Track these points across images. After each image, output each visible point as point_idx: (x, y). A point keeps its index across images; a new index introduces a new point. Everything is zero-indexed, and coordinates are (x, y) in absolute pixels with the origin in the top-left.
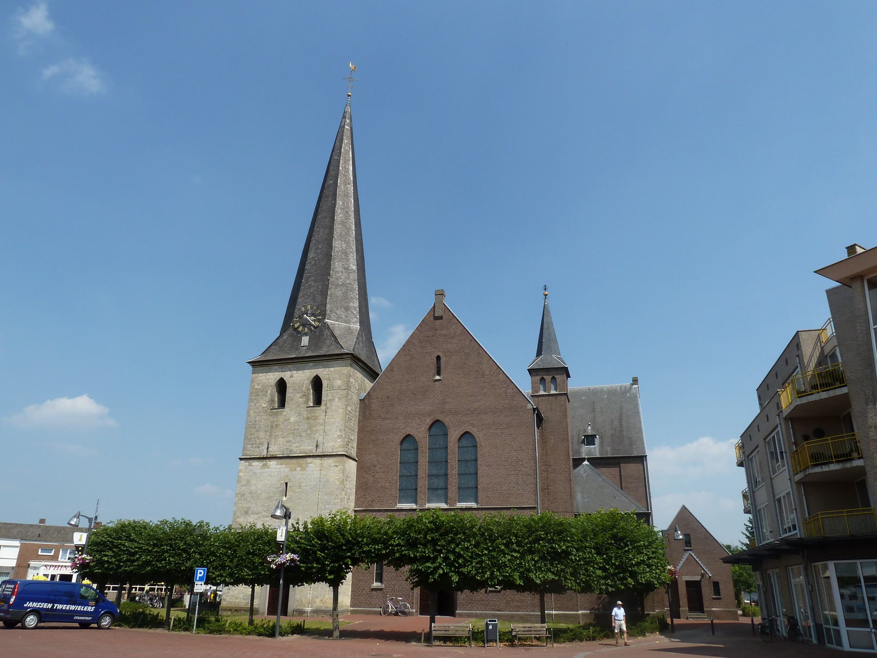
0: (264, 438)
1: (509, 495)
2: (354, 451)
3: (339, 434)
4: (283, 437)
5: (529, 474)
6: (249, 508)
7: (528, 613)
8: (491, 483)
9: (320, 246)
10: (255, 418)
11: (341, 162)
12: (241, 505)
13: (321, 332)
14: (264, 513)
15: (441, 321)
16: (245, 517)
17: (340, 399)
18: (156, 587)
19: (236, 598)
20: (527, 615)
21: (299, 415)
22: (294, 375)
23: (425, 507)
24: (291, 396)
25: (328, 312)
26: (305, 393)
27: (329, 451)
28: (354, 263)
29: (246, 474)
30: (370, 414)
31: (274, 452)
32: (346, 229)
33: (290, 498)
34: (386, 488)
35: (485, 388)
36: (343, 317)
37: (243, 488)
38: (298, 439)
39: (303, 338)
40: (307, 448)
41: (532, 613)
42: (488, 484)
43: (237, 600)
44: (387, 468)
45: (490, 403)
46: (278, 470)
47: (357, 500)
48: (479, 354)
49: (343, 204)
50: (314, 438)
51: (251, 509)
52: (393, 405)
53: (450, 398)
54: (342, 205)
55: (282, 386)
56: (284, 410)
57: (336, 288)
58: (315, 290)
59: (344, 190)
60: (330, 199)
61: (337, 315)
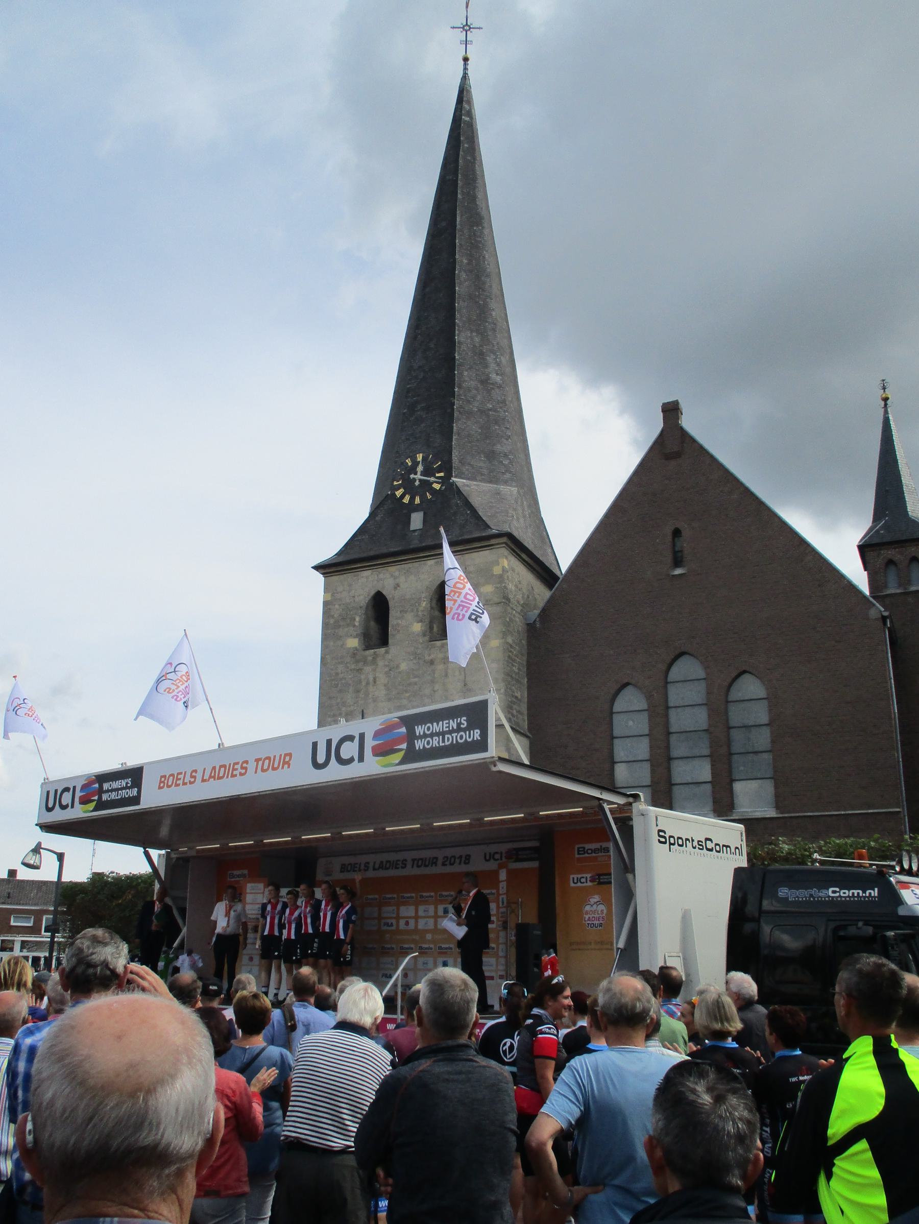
36: (485, 471)
57: (468, 418)
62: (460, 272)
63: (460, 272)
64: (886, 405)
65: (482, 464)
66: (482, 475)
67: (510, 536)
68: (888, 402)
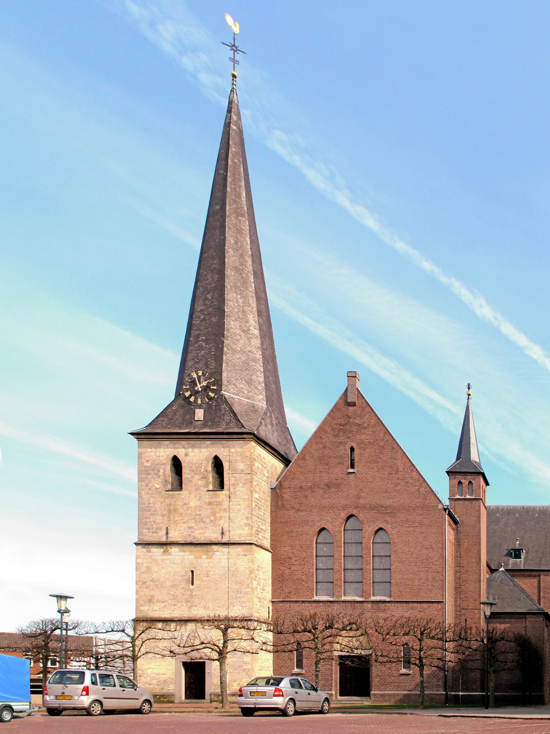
3: (246, 522)
4: (184, 523)
5: (438, 572)
8: (403, 578)
9: (209, 297)
10: (149, 500)
11: (229, 180)
12: (143, 593)
13: (218, 405)
15: (355, 408)
17: (244, 484)
19: (150, 684)
20: (432, 694)
21: (200, 499)
22: (190, 454)
25: (225, 382)
26: (204, 474)
27: (237, 539)
28: (254, 326)
29: (145, 560)
30: (282, 504)
31: (175, 538)
33: (198, 587)
34: (303, 581)
35: (399, 485)
37: (144, 576)
38: (202, 525)
39: (197, 411)
41: (437, 692)
43: (151, 686)
45: (403, 501)
46: (181, 557)
47: (274, 592)
48: (393, 448)
49: (236, 242)
50: (219, 525)
52: (306, 496)
53: (364, 492)
56: (181, 492)
58: (208, 354)
60: (217, 232)
61: (237, 388)
62: (229, 248)
63: (229, 248)
64: (468, 398)
66: (243, 393)
67: (253, 434)
68: (470, 397)
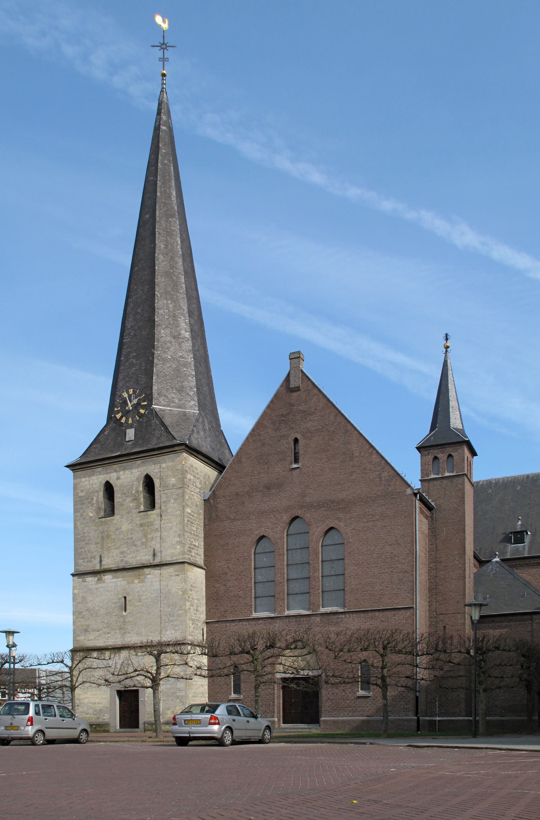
0: (96, 551)
1: (381, 596)
2: (201, 558)
3: (178, 539)
4: (117, 548)
6: (88, 626)
7: (400, 717)
9: (139, 310)
10: (83, 530)
14: (104, 630)
15: (299, 393)
16: (85, 635)
17: (175, 499)
18: (276, 719)
19: (87, 714)
22: (122, 477)
23: (285, 614)
24: (120, 502)
25: (155, 395)
26: (135, 496)
27: (169, 559)
28: (185, 329)
30: (217, 515)
31: (108, 565)
32: (173, 282)
33: (131, 613)
34: (240, 597)
39: (128, 431)
40: (144, 558)
42: (356, 585)
43: (88, 716)
44: (240, 575)
46: (114, 584)
50: (151, 547)
51: (91, 627)
52: (243, 503)
54: (164, 248)
55: (109, 489)
56: (114, 517)
59: (166, 226)
61: (168, 398)
62: (159, 255)
64: (446, 351)
65: (173, 395)
